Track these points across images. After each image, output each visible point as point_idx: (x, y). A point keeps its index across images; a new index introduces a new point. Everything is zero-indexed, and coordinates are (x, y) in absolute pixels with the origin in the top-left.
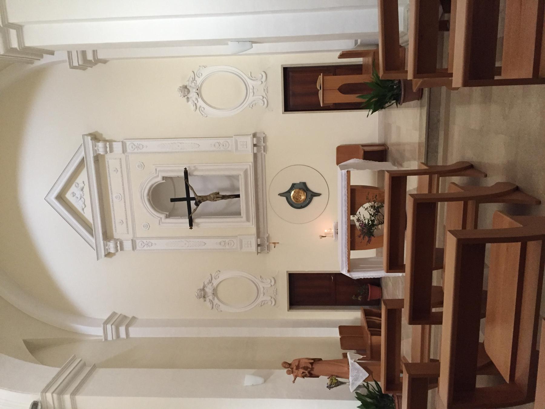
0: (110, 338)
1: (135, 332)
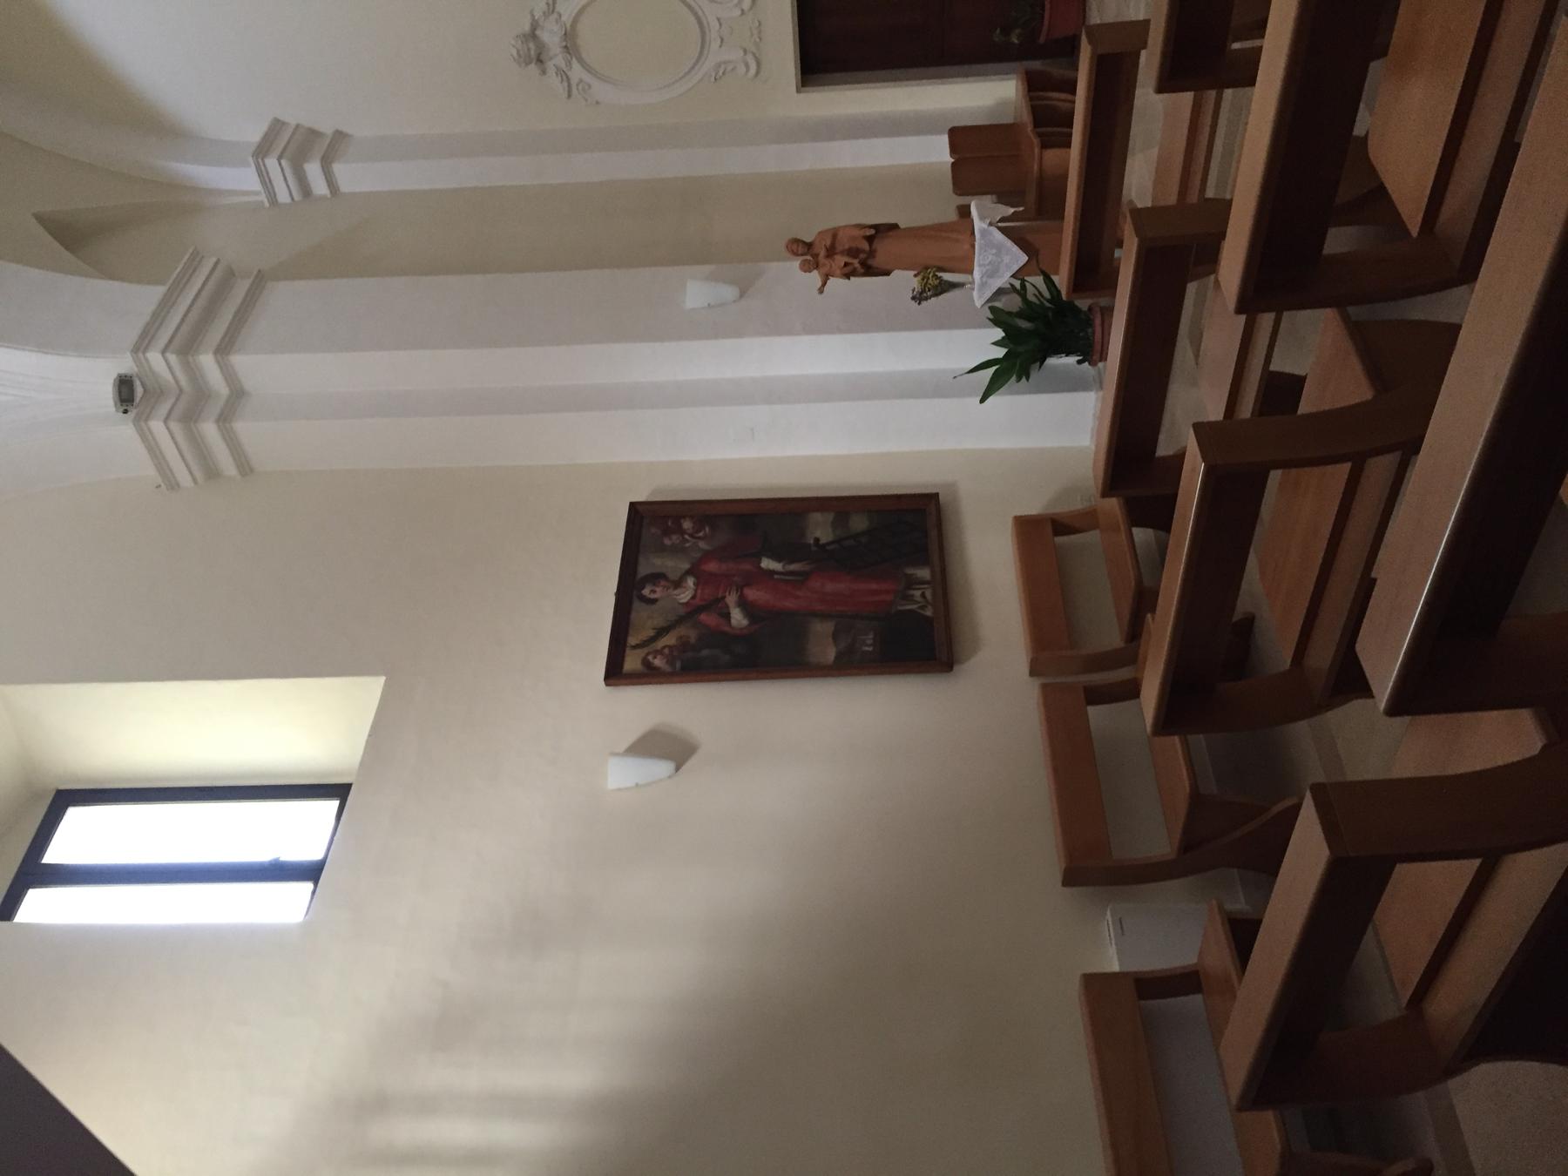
0: (283, 196)
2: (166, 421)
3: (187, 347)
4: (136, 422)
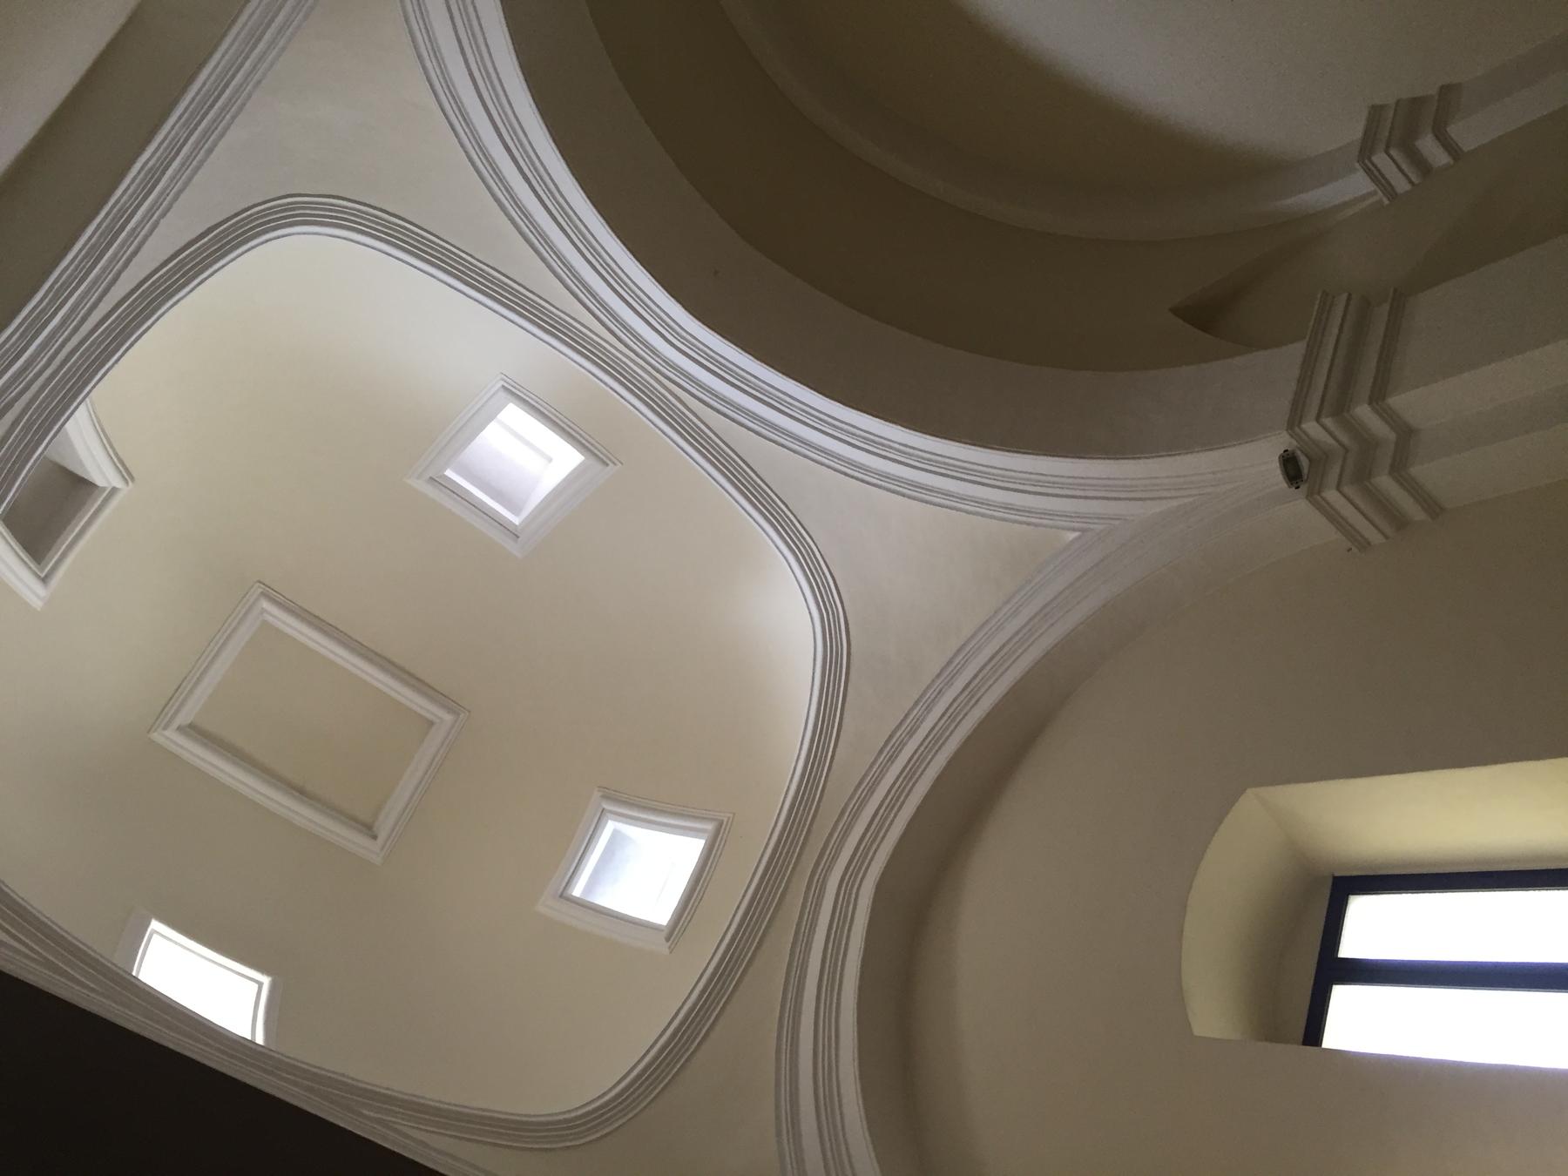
0: (1401, 185)
1: (1471, 132)
2: (1338, 488)
3: (1339, 407)
4: (1309, 496)
